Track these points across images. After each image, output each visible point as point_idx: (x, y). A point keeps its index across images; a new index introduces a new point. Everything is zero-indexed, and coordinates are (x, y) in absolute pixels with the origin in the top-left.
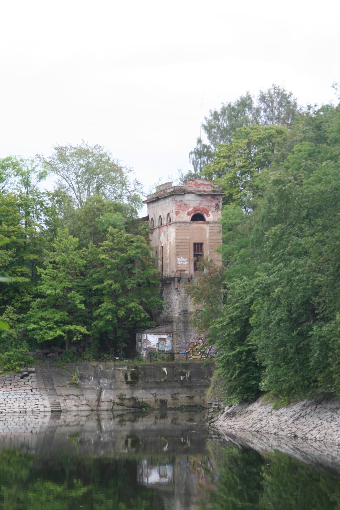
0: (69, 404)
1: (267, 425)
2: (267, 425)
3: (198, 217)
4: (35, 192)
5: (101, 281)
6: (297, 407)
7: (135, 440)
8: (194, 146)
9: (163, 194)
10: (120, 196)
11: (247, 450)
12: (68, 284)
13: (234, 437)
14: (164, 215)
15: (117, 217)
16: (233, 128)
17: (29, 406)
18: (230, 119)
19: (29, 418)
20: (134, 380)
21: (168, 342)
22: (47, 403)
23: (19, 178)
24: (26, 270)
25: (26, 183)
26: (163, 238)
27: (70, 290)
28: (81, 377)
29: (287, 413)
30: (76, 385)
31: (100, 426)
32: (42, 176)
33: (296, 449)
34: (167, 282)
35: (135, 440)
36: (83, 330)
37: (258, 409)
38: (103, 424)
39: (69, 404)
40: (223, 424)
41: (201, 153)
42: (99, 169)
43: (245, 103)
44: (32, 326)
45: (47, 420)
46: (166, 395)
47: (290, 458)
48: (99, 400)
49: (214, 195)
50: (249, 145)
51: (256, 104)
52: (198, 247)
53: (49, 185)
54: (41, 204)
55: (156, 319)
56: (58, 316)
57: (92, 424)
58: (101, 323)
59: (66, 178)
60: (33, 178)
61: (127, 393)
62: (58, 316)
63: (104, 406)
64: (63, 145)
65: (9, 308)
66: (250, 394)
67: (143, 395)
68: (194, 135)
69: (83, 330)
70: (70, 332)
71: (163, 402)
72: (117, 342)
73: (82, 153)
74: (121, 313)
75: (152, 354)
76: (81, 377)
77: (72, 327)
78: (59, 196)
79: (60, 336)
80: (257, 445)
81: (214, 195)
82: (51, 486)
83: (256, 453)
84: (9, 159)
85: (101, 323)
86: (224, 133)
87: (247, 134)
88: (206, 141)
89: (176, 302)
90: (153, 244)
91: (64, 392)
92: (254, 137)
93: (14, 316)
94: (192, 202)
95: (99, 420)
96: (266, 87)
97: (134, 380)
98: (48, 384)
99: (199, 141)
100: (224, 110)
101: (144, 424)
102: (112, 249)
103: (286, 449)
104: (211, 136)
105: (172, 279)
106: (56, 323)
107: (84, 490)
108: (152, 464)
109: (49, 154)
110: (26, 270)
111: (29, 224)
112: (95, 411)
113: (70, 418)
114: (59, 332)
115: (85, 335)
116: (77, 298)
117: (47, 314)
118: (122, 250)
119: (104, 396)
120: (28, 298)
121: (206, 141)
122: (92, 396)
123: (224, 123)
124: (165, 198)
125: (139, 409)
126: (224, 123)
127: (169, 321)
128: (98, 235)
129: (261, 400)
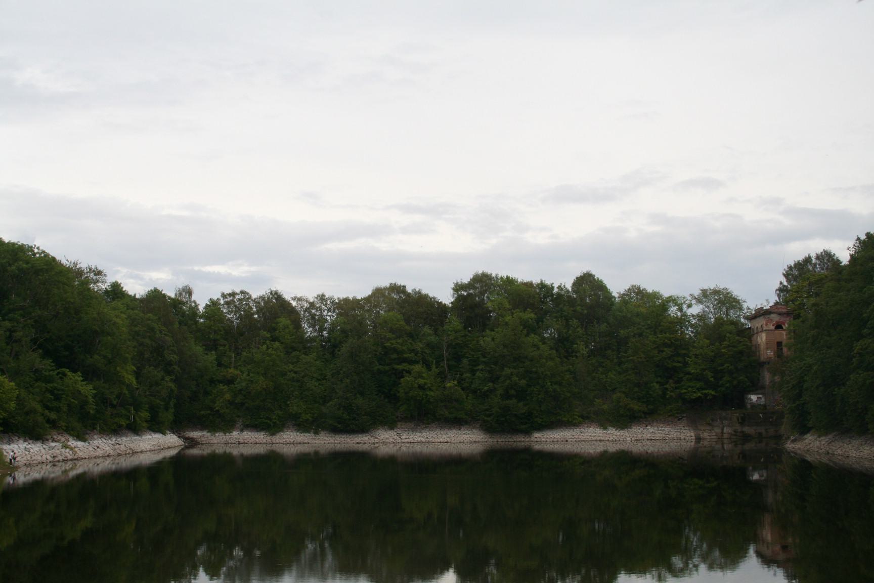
0: (706, 435)
1: (813, 446)
2: (813, 446)
3: (779, 327)
4: (684, 315)
5: (723, 365)
6: (830, 436)
7: (744, 455)
8: (777, 286)
9: (761, 313)
10: (739, 316)
11: (804, 461)
12: (703, 367)
13: (796, 454)
14: (759, 326)
15: (732, 327)
16: (800, 275)
17: (682, 436)
18: (799, 270)
19: (683, 443)
20: (743, 421)
21: (763, 399)
22: (692, 434)
23: (676, 308)
24: (680, 359)
25: (681, 310)
26: (759, 339)
27: (704, 370)
28: (713, 420)
29: (824, 440)
30: (709, 424)
31: (723, 447)
32: (689, 306)
33: (830, 460)
34: (762, 364)
35: (744, 455)
36: (713, 393)
37: (809, 438)
38: (726, 446)
39: (706, 435)
40: (789, 446)
41: (782, 290)
42: (725, 300)
43: (808, 260)
44: (684, 391)
45: (693, 444)
46: (762, 430)
47: (827, 465)
48: (722, 433)
49: (788, 314)
50: (809, 285)
51: (814, 261)
52: (779, 344)
53: (696, 310)
54: (689, 321)
55: (755, 387)
56: (699, 385)
57: (719, 446)
58: (723, 389)
59: (708, 307)
60: (685, 307)
61: (738, 428)
62: (699, 385)
63: (726, 436)
64: (706, 288)
65: (671, 381)
66: (803, 429)
67: (747, 430)
68: (778, 279)
69: (713, 393)
70: (705, 394)
71: (760, 434)
72: (732, 399)
73: (716, 292)
74: (735, 382)
75: (753, 406)
76: (713, 420)
77: (706, 391)
78: (702, 317)
79: (700, 397)
80: (809, 458)
81: (788, 314)
82: (696, 480)
83: (808, 462)
84: (670, 297)
85: (723, 389)
86: (795, 278)
87: (808, 279)
88: (785, 283)
89: (767, 377)
90: (754, 343)
91: (703, 428)
92: (812, 280)
93: (673, 385)
94: (775, 318)
95: (723, 444)
96: (820, 251)
97: (743, 421)
98: (693, 424)
99: (781, 283)
100: (795, 265)
101: (748, 446)
102: (729, 346)
103: (825, 460)
104: (788, 280)
105: (764, 363)
106: (698, 389)
107: (715, 483)
108: (755, 469)
109: (697, 293)
110: (680, 359)
111: (682, 333)
112: (720, 439)
113: (706, 443)
114: (699, 394)
115: (714, 396)
116: (709, 375)
117: (691, 384)
118: (734, 347)
119: (725, 430)
120: (681, 375)
121: (785, 283)
122: (718, 430)
123: (795, 272)
124: (760, 316)
125: (746, 438)
126: (795, 272)
127: (763, 387)
128: (721, 338)
129: (811, 432)
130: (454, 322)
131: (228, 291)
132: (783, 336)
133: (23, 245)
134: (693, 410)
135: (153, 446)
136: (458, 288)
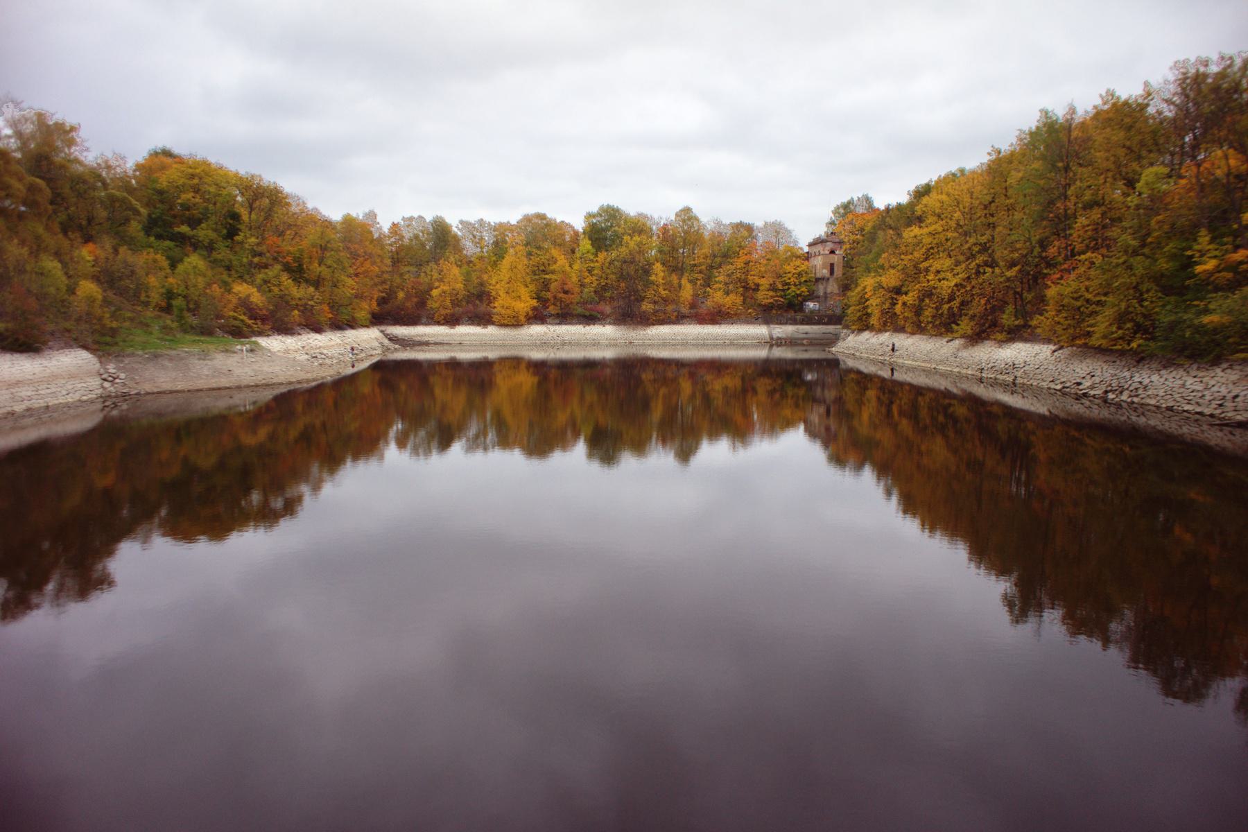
3: (832, 252)
52: (832, 265)
55: (812, 296)
75: (812, 312)
126: (842, 211)
130: (586, 245)
131: (407, 215)
132: (835, 259)
133: (745, 230)
134: (767, 314)
135: (366, 343)
136: (590, 216)
